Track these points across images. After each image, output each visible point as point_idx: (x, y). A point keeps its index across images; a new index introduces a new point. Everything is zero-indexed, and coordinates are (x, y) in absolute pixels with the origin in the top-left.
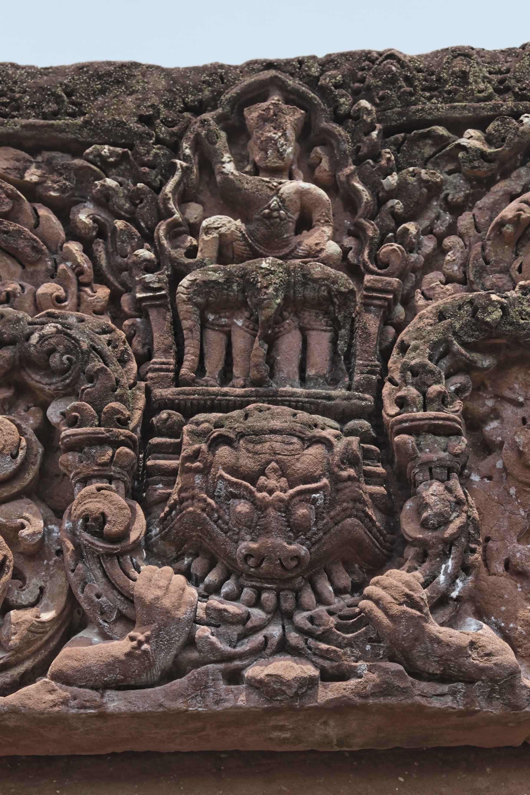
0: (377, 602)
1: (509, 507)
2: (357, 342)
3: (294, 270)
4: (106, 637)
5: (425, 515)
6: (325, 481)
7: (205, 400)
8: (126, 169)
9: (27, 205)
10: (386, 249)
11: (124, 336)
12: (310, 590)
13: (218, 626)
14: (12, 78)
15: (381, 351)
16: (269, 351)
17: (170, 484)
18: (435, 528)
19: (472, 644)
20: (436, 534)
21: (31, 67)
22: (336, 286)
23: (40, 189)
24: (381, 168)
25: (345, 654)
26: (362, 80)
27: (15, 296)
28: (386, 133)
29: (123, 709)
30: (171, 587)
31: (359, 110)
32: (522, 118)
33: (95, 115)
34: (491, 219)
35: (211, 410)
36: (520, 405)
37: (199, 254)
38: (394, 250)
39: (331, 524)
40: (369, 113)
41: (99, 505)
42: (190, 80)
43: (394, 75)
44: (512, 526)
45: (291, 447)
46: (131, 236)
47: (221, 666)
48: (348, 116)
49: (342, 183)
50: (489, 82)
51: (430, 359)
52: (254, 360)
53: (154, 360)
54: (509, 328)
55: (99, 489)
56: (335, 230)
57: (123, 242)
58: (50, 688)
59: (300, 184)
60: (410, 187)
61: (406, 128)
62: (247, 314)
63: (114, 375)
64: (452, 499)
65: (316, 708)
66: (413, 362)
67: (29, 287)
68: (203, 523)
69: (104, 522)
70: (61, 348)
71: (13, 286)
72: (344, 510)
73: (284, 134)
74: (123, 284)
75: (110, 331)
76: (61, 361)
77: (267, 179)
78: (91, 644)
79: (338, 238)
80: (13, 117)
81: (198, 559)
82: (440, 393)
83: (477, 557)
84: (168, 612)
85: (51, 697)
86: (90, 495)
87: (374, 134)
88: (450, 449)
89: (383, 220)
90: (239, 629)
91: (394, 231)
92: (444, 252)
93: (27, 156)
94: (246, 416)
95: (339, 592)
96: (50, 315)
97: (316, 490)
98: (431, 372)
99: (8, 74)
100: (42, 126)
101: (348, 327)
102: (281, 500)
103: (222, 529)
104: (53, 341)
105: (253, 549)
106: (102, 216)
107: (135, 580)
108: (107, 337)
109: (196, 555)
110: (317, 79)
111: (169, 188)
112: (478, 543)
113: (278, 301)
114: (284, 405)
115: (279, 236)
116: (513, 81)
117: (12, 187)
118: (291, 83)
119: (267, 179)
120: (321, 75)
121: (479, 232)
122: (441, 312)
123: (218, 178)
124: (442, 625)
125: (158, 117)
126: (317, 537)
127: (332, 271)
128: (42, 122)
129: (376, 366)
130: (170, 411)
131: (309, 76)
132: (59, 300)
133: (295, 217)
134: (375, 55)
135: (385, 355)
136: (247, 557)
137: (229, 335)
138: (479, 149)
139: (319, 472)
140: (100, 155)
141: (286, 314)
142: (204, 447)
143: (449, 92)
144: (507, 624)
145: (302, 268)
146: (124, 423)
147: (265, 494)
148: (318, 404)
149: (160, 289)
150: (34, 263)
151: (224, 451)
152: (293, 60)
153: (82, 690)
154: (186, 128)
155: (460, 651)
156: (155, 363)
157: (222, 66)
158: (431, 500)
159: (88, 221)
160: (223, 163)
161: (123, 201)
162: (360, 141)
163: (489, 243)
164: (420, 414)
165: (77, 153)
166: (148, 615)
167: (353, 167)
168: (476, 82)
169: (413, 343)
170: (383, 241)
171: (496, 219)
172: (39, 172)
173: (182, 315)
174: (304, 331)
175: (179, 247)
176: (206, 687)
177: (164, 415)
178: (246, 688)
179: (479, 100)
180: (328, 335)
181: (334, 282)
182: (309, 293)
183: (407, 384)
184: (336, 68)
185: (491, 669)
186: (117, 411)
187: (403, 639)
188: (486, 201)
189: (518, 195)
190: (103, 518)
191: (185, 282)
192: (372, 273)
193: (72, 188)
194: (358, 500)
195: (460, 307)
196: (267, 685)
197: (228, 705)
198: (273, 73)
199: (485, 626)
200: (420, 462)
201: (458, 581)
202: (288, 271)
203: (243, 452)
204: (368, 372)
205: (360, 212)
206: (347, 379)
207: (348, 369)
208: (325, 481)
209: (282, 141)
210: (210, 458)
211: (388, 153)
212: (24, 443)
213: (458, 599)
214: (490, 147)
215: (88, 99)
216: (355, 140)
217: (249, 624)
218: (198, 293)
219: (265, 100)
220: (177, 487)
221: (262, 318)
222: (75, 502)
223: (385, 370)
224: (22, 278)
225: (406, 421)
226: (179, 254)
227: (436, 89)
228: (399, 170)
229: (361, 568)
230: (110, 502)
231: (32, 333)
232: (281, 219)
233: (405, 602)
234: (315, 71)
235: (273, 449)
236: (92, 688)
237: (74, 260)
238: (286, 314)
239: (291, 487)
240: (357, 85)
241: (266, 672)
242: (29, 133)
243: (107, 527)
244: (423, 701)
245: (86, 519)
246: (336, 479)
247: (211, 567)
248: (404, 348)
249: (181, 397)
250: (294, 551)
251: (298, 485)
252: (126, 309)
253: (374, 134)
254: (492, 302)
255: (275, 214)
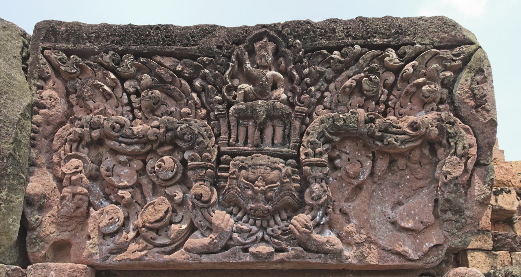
0: (295, 226)
1: (342, 190)
2: (292, 131)
3: (270, 105)
4: (204, 236)
5: (313, 195)
6: (278, 183)
7: (238, 152)
8: (212, 66)
9: (177, 79)
10: (304, 96)
11: (210, 128)
12: (273, 220)
13: (240, 233)
14: (172, 30)
15: (300, 134)
16: (261, 134)
17: (226, 182)
18: (316, 200)
19: (327, 241)
20: (316, 202)
21: (179, 26)
22: (285, 111)
23: (182, 74)
24: (303, 66)
25: (283, 244)
26: (297, 32)
27: (173, 113)
28: (305, 52)
29: (208, 261)
30: (224, 220)
31: (296, 44)
32: (354, 47)
33: (201, 45)
34: (341, 86)
35: (240, 155)
36: (348, 154)
37: (237, 98)
38: (306, 97)
39: (280, 198)
40: (299, 45)
41: (200, 191)
42: (235, 32)
43: (309, 30)
44: (342, 197)
45: (267, 171)
46: (214, 91)
47: (241, 247)
48: (292, 46)
49: (289, 71)
50: (343, 33)
51: (317, 139)
52: (256, 138)
53: (221, 137)
54: (346, 127)
55: (200, 185)
56: (285, 90)
57: (211, 93)
58: (183, 253)
59: (273, 72)
60: (313, 73)
61: (313, 51)
62: (253, 121)
63: (206, 143)
64: (323, 190)
65: (273, 262)
66: (311, 140)
67: (178, 109)
68: (236, 197)
69: (202, 197)
70: (188, 133)
71: (172, 109)
72: (285, 193)
73: (268, 53)
74: (211, 108)
75: (206, 126)
76: (188, 137)
77: (262, 70)
78: (198, 238)
79: (286, 92)
80: (172, 46)
81: (235, 208)
82: (320, 151)
83: (330, 210)
84: (223, 229)
85: (184, 257)
86: (197, 187)
87: (301, 53)
88: (323, 172)
89: (303, 86)
90: (248, 234)
91: (306, 90)
92: (324, 98)
93: (177, 60)
94: (252, 159)
95: (282, 220)
96: (185, 120)
97: (275, 187)
98: (317, 144)
99: (170, 29)
100: (182, 49)
101: (289, 125)
102: (263, 190)
103: (242, 199)
104: (185, 130)
105: (253, 207)
106: (204, 83)
107: (212, 216)
108: (204, 128)
109: (235, 206)
110: (281, 31)
111: (227, 73)
112: (331, 205)
113: (264, 116)
114: (265, 154)
115: (265, 92)
116: (352, 32)
117: (172, 72)
118: (271, 33)
119: (262, 70)
120: (282, 30)
121: (336, 90)
122: (322, 121)
123: (244, 70)
124: (317, 233)
125: (224, 46)
126: (275, 203)
127: (283, 105)
128: (182, 47)
129: (298, 140)
130: (226, 156)
131: (278, 30)
132: (189, 114)
133: (271, 85)
134: (302, 22)
135: (301, 136)
136: (251, 209)
137: (247, 128)
138: (338, 59)
139: (276, 180)
140: (203, 61)
141: (267, 120)
142: (237, 170)
143: (328, 36)
144: (339, 232)
145: (273, 104)
146: (209, 160)
147: (257, 188)
148: (277, 154)
149: (223, 111)
150: (180, 100)
151: (243, 172)
152: (272, 24)
153: (194, 254)
154: (234, 50)
155: (323, 244)
156: (221, 138)
157: (247, 27)
158: (316, 190)
159: (199, 85)
160: (246, 64)
161: (211, 78)
162: (296, 55)
163: (340, 95)
164: (312, 159)
165: (195, 60)
166: (216, 230)
167: (293, 66)
168: (338, 32)
169: (311, 132)
170: (302, 93)
171: (343, 86)
172: (182, 67)
173: (231, 121)
174: (274, 126)
175: (231, 95)
176: (236, 254)
177: (224, 157)
178: (250, 255)
179: (339, 40)
180: (282, 128)
181: (284, 110)
182: (275, 113)
183: (309, 148)
184: (288, 27)
185: (333, 250)
186: (207, 156)
187: (304, 240)
188: (340, 78)
189: (351, 77)
190: (201, 195)
191: (232, 109)
192: (298, 105)
193: (193, 73)
194: (290, 190)
195: (329, 119)
196: (256, 255)
197: (243, 260)
198: (265, 29)
199: (332, 233)
200: (312, 176)
201: (323, 218)
202: (268, 105)
203: (250, 173)
204: (295, 142)
205: (295, 82)
206: (288, 144)
207: (289, 140)
208: (278, 183)
209: (267, 56)
210: (239, 174)
211: (305, 60)
212: (176, 166)
213: (323, 224)
214: (342, 58)
215: (199, 39)
216: (294, 55)
217: (251, 232)
218: (236, 113)
219: (262, 40)
220: (228, 183)
221: (258, 123)
222: (192, 189)
223: (301, 142)
224: (176, 106)
225: (307, 162)
226: (230, 98)
227: (324, 35)
228: (309, 67)
229: (290, 211)
230: (204, 189)
231: (178, 127)
232: (266, 86)
233: (305, 227)
234: (280, 28)
235: (260, 171)
236: (197, 254)
237: (194, 99)
238: (267, 120)
239: (267, 185)
240: (295, 33)
241: (256, 250)
242: (178, 52)
243: (202, 198)
244: (309, 260)
245: (195, 195)
246: (282, 183)
247: (239, 211)
248: (308, 134)
249: (230, 151)
250: (267, 208)
251: (269, 184)
252: (212, 118)
253: (301, 53)
254: (340, 118)
255: (264, 83)
